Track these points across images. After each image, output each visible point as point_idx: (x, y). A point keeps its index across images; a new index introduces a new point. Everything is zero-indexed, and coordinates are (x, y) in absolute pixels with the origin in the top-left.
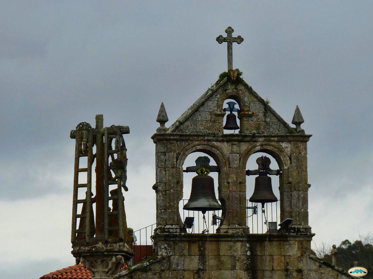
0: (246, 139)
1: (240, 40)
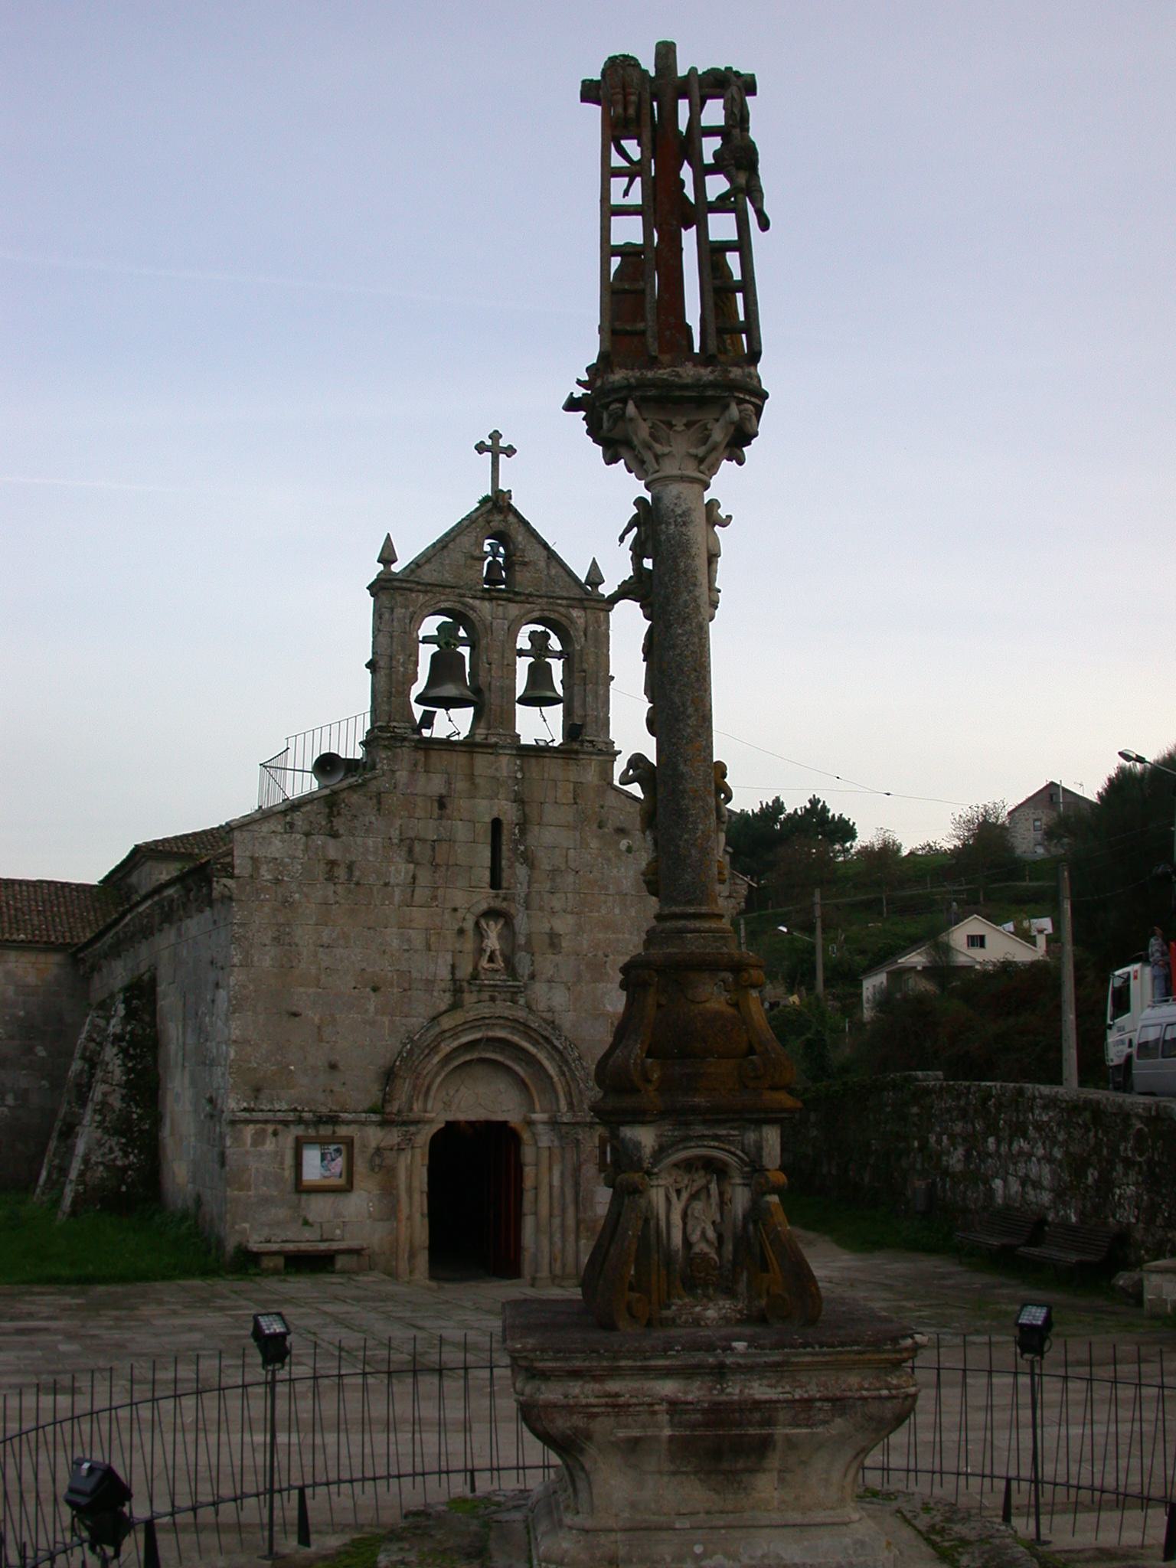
0: (518, 598)
1: (510, 451)
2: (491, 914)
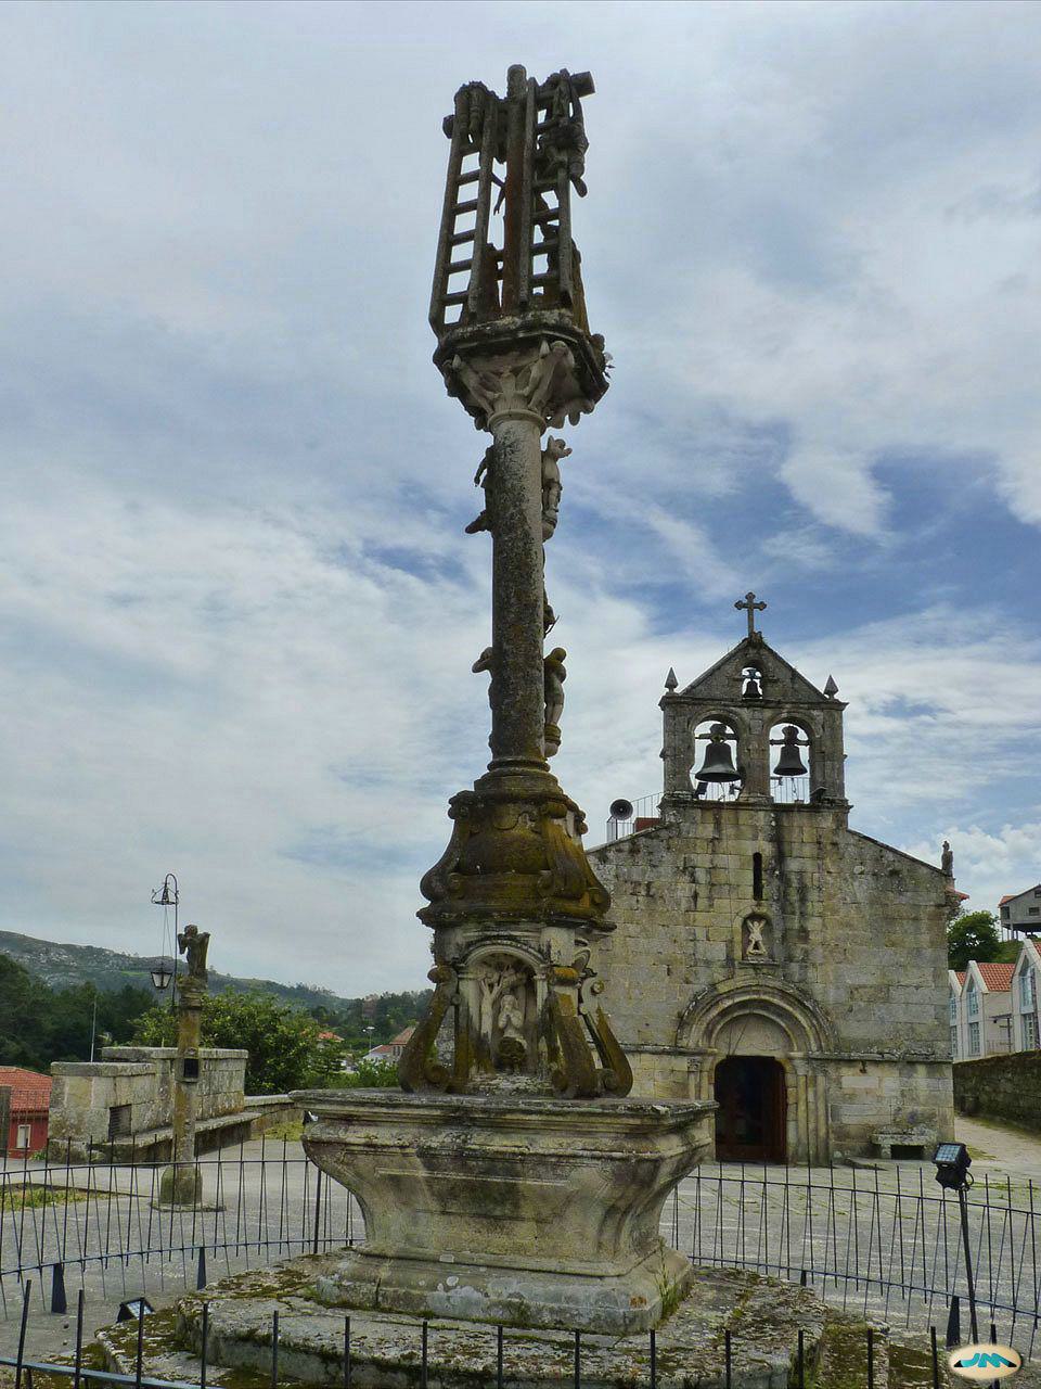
1: (762, 606)
2: (754, 917)
